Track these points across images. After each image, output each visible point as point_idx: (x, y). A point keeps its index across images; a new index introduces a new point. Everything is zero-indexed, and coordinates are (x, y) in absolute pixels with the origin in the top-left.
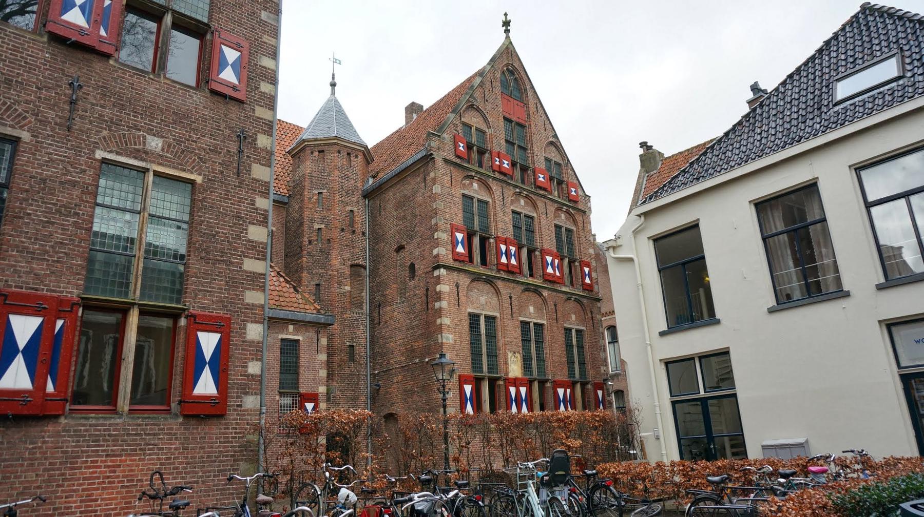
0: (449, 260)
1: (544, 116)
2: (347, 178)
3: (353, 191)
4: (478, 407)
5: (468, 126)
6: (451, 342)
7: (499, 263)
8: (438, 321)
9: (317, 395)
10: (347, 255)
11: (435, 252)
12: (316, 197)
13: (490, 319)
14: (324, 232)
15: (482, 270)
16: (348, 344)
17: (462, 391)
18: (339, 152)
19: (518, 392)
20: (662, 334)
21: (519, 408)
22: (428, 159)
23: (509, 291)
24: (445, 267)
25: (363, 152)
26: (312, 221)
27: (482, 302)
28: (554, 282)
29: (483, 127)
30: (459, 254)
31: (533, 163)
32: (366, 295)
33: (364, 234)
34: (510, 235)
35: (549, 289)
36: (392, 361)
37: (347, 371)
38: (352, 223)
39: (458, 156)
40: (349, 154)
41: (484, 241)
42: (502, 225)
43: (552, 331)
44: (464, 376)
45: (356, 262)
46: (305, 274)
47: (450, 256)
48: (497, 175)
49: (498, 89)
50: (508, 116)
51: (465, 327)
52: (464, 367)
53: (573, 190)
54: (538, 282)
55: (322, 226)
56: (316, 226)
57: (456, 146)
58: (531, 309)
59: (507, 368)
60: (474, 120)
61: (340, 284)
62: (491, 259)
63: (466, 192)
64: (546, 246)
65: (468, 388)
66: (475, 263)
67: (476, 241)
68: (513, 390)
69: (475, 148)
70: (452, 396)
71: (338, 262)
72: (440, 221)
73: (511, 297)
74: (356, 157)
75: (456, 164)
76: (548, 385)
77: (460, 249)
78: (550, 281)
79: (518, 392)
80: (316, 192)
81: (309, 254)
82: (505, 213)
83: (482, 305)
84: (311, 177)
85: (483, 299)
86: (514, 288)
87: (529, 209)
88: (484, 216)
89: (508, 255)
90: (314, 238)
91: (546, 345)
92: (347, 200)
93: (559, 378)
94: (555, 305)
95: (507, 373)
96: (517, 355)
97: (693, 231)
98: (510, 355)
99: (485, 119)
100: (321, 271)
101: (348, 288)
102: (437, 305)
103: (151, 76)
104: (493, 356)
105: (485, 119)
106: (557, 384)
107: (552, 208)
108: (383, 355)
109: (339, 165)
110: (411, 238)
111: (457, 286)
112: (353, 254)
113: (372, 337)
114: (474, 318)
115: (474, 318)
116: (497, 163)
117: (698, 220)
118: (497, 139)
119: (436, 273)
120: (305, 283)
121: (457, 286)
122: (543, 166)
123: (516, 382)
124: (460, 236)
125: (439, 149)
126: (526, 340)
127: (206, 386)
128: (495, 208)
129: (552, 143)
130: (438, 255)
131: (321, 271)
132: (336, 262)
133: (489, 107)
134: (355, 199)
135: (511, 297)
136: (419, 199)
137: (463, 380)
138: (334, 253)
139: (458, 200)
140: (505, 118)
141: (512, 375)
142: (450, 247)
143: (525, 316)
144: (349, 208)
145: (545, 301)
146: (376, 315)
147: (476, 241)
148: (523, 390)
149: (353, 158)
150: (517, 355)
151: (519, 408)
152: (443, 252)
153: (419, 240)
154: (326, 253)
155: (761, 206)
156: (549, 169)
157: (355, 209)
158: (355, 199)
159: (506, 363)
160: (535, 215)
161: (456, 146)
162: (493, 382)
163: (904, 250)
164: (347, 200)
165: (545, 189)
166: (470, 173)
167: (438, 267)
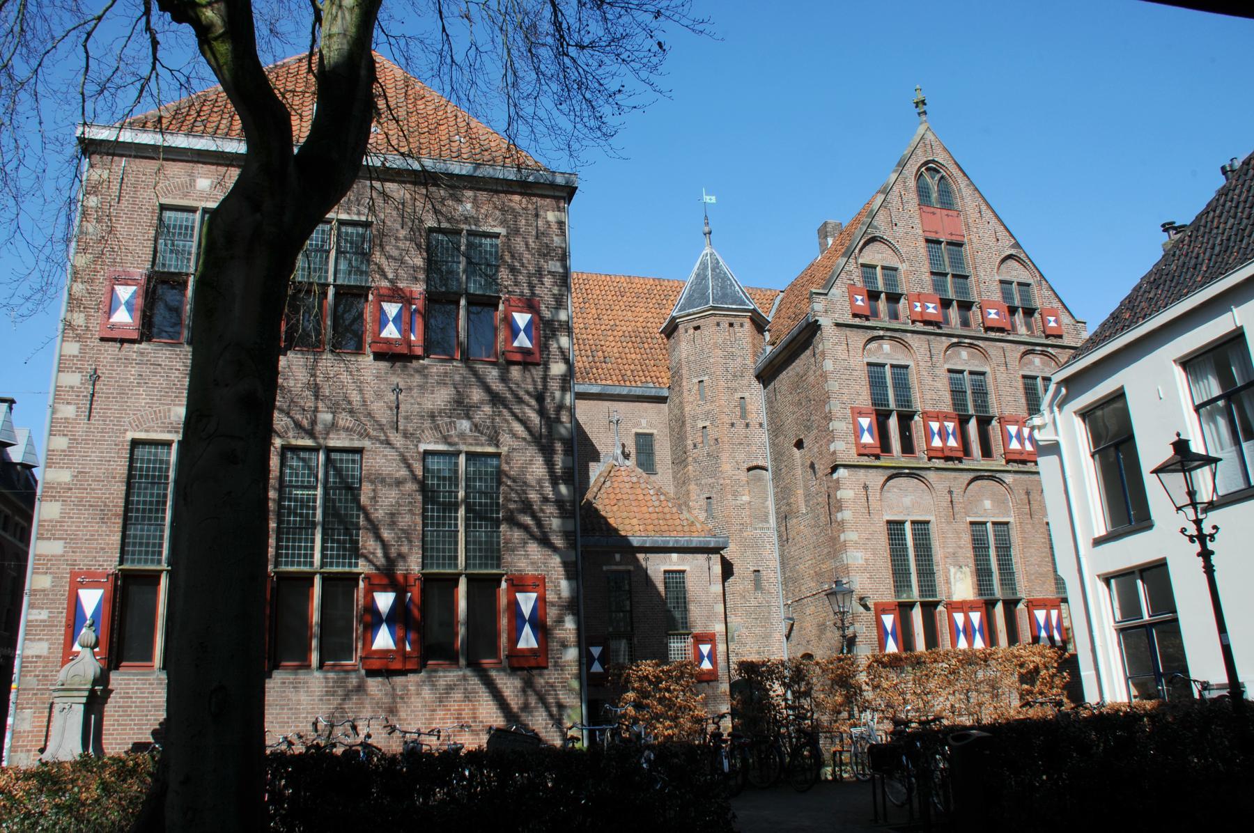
0: (852, 457)
1: (994, 221)
2: (732, 356)
3: (742, 372)
4: (991, 639)
5: (868, 268)
6: (861, 562)
7: (930, 449)
8: (842, 537)
9: (714, 635)
10: (741, 456)
11: (832, 448)
12: (696, 387)
13: (921, 527)
14: (710, 431)
15: (905, 461)
16: (752, 569)
17: (880, 625)
18: (718, 324)
19: (968, 621)
20: (1098, 542)
21: (970, 641)
22: (811, 330)
23: (947, 484)
24: (845, 466)
25: (751, 319)
26: (695, 418)
27: (907, 501)
28: (1024, 462)
29: (893, 261)
30: (865, 446)
31: (980, 294)
32: (771, 504)
33: (761, 425)
34: (946, 406)
35: (1016, 472)
36: (803, 588)
37: (754, 603)
38: (744, 415)
39: (855, 315)
40: (731, 325)
41: (906, 419)
42: (931, 393)
43: (1023, 531)
44: (882, 604)
45: (754, 463)
46: (692, 487)
47: (854, 451)
48: (919, 327)
49: (912, 198)
50: (932, 236)
51: (882, 540)
52: (885, 592)
53: (1052, 319)
54: (998, 463)
55: (707, 424)
56: (701, 425)
57: (852, 301)
58: (988, 504)
59: (949, 588)
60: (875, 255)
61: (735, 494)
62: (919, 442)
63: (873, 360)
64: (1008, 411)
65: (888, 620)
66: (895, 453)
67: (893, 423)
68: (959, 618)
69: (883, 296)
70: (670, 732)
71: (731, 466)
72: (835, 406)
73: (950, 492)
74: (742, 325)
75: (861, 322)
76: (1021, 606)
77: (867, 439)
78: (1015, 461)
79: (968, 621)
80: (696, 380)
81: (695, 460)
82: (934, 377)
83: (907, 508)
84: (688, 362)
85: (907, 501)
86: (955, 478)
87: (976, 362)
88: (903, 386)
89: (937, 435)
90: (699, 440)
91: (1015, 553)
92: (734, 384)
93: (1037, 595)
94: (1028, 493)
95: (949, 596)
96: (965, 569)
97: (1118, 405)
98: (953, 570)
99: (895, 251)
100: (711, 481)
101: (746, 498)
102: (839, 516)
103: (508, 258)
104: (927, 573)
105: (895, 251)
106: (1032, 605)
107: (1015, 352)
108: (795, 581)
109: (720, 341)
110: (808, 428)
111: (866, 487)
112: (749, 454)
113: (782, 556)
114: (895, 528)
115: (895, 528)
116: (919, 309)
117: (1122, 387)
118: (915, 274)
119: (835, 476)
120: (693, 496)
121: (866, 487)
122: (997, 296)
123: (964, 607)
124: (865, 422)
125: (826, 311)
126: (979, 546)
127: (528, 640)
128: (918, 372)
129: (1010, 257)
130: (834, 453)
131: (711, 481)
132: (727, 467)
133: (900, 231)
134: (745, 382)
135: (950, 492)
136: (811, 379)
137: (882, 609)
138: (724, 457)
139: (862, 375)
140: (927, 241)
141: (957, 598)
142: (852, 439)
143: (976, 514)
144: (740, 395)
145: (1009, 489)
146: (783, 529)
147: (893, 423)
148: (976, 617)
149: (737, 328)
150: (965, 569)
151: (970, 641)
152: (844, 449)
153: (815, 431)
154: (714, 456)
155: (1190, 364)
156: (1007, 295)
157: (746, 395)
158: (745, 382)
159: (948, 582)
160: (987, 369)
161: (852, 301)
162: (929, 608)
163: (931, 526)
164: (734, 384)
165: (1001, 330)
166: (876, 333)
167: (834, 469)
